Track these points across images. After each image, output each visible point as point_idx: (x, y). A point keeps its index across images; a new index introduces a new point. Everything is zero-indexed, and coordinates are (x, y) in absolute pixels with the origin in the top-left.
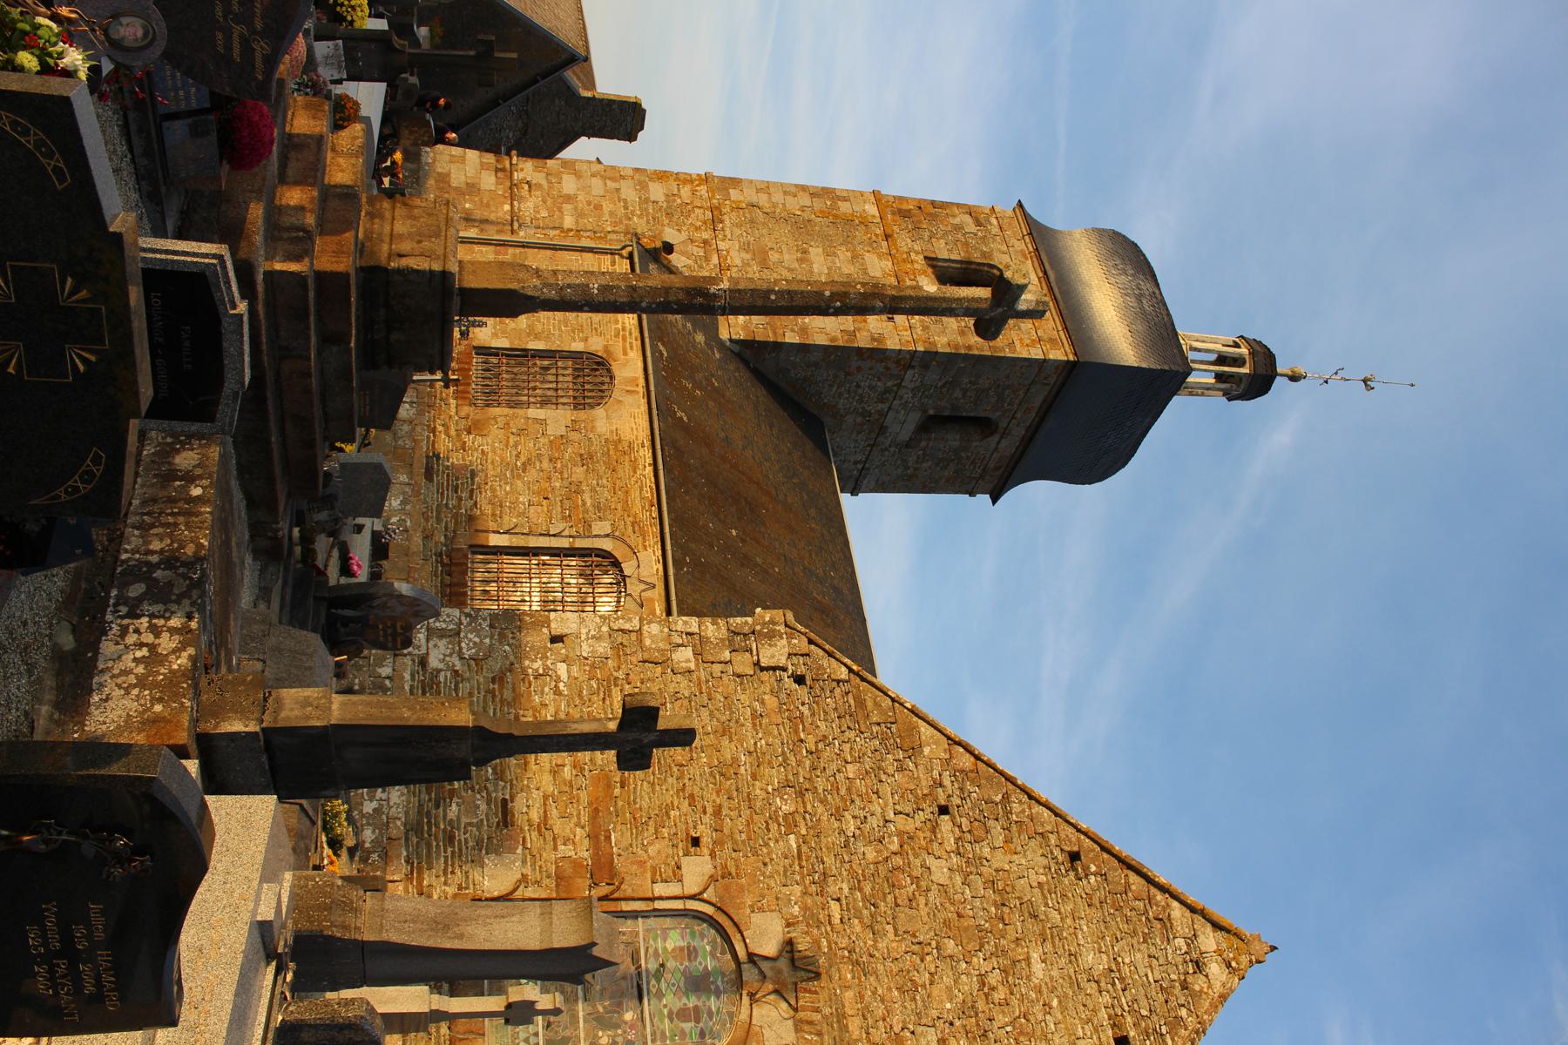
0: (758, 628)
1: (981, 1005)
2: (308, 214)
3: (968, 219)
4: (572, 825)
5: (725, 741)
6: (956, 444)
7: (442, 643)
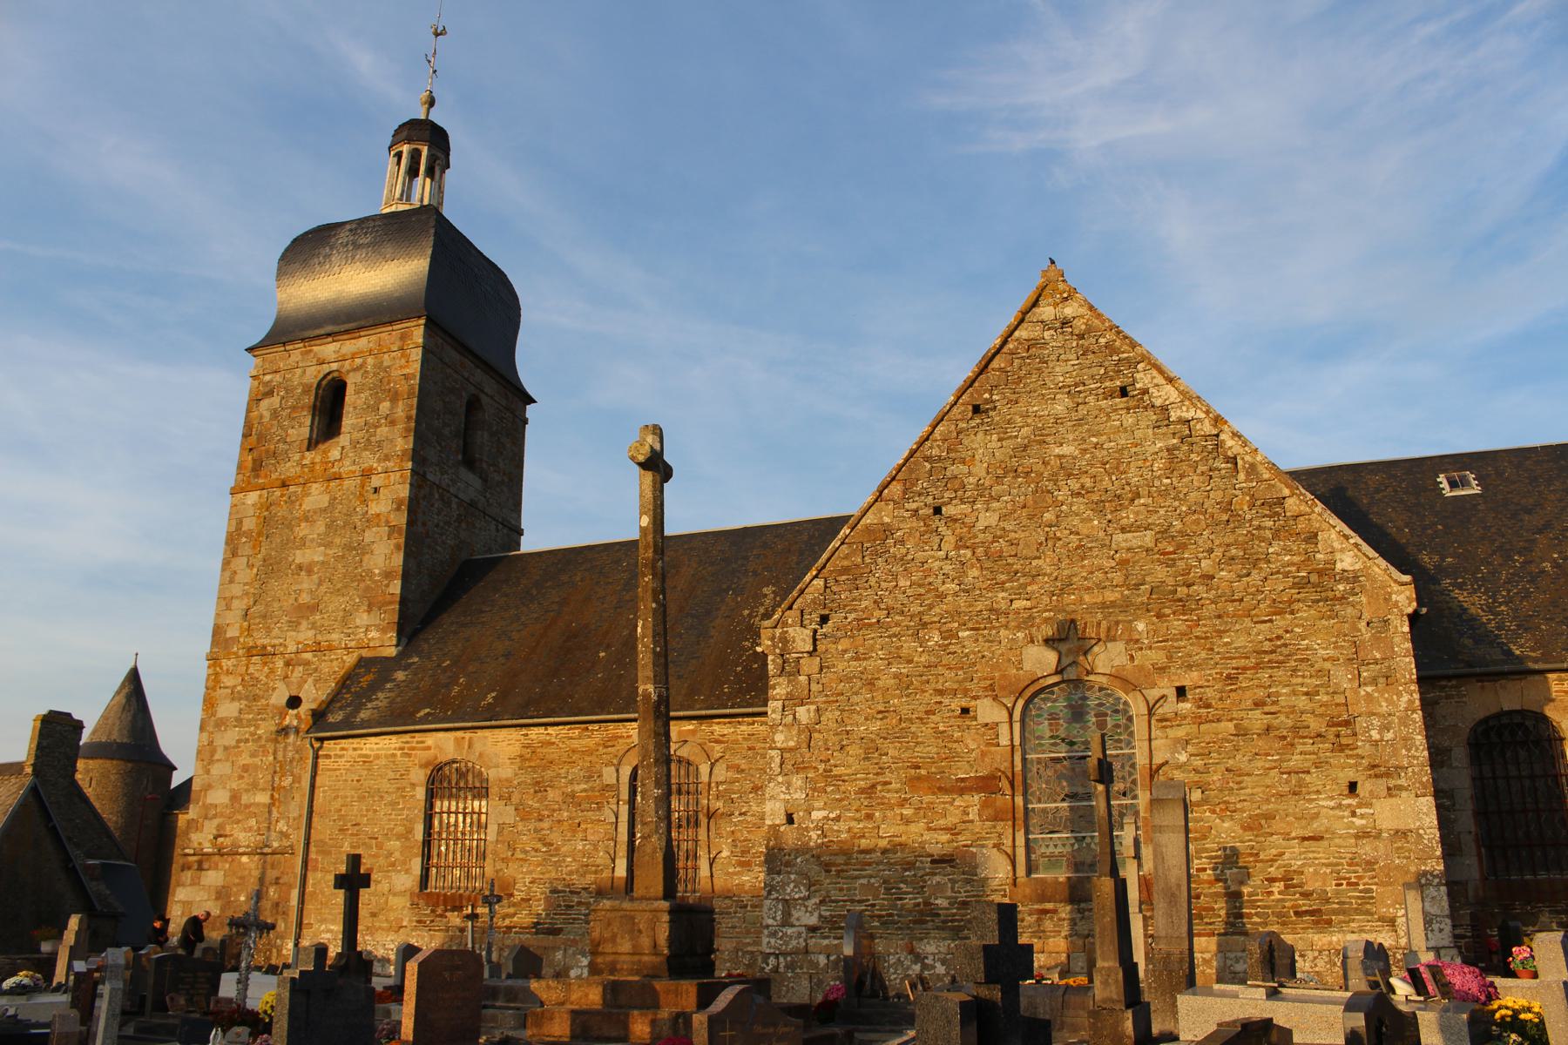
0: (778, 651)
1: (1095, 497)
2: (659, 1016)
3: (265, 404)
4: (952, 808)
5: (880, 683)
6: (486, 435)
7: (795, 914)
